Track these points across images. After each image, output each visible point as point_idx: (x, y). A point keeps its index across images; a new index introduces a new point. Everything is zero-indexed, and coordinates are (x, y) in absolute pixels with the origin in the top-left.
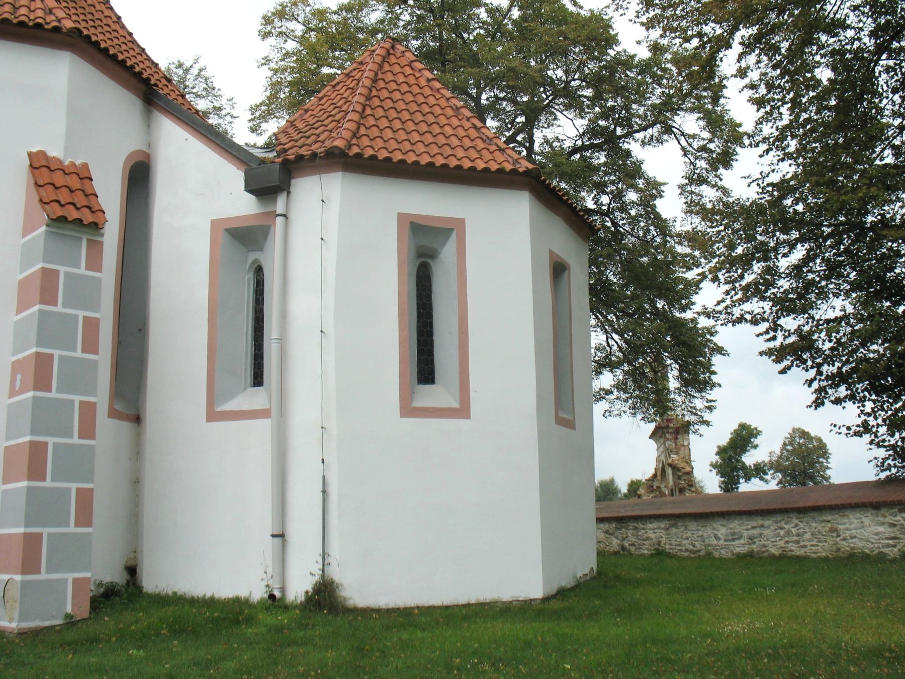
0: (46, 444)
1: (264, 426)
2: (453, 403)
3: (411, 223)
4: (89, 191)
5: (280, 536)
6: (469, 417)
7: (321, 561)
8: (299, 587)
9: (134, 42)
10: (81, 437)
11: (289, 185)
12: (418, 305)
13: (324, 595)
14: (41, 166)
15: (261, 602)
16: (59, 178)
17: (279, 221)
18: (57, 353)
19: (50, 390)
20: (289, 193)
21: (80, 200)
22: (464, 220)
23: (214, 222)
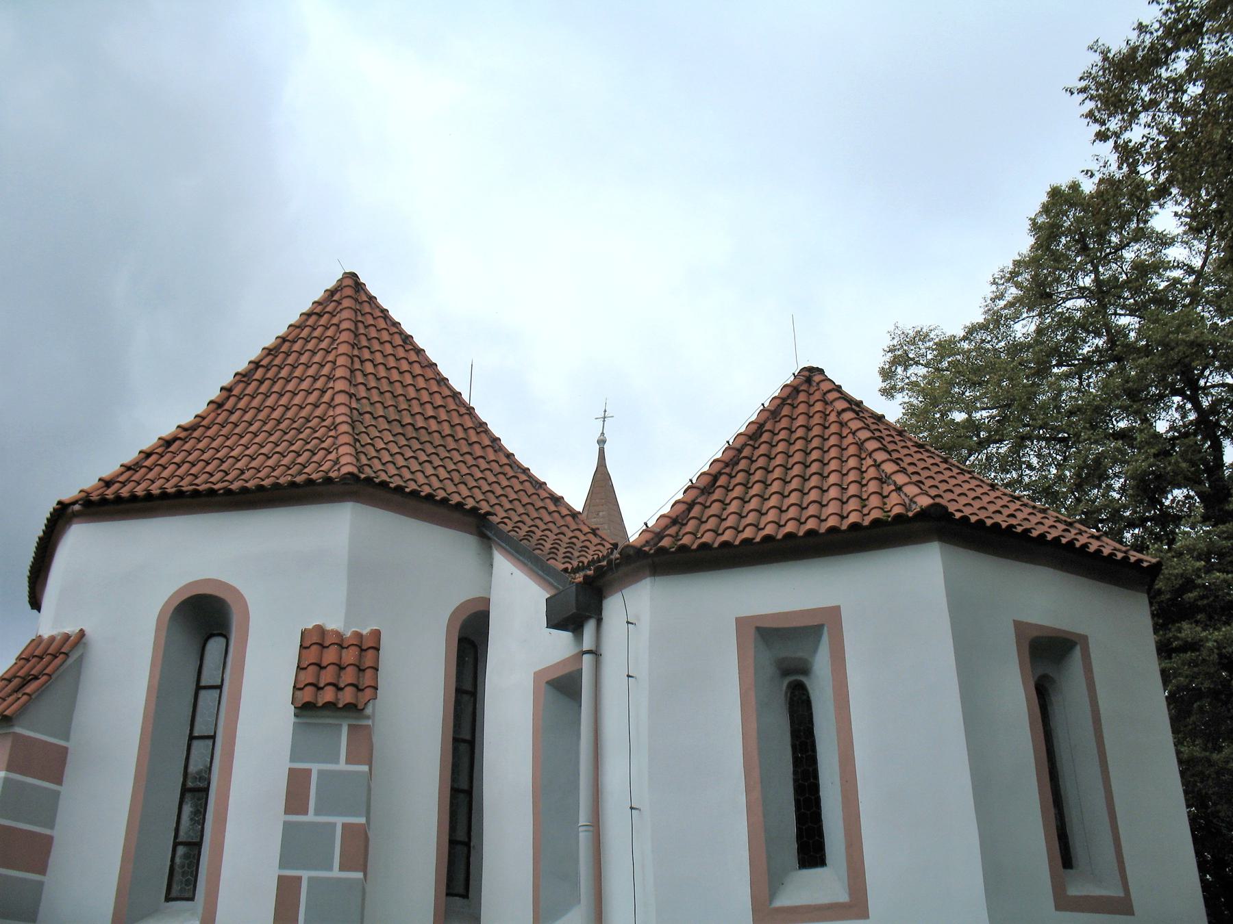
3: (758, 629)
12: (794, 747)
14: (315, 643)
17: (587, 659)
22: (737, 619)
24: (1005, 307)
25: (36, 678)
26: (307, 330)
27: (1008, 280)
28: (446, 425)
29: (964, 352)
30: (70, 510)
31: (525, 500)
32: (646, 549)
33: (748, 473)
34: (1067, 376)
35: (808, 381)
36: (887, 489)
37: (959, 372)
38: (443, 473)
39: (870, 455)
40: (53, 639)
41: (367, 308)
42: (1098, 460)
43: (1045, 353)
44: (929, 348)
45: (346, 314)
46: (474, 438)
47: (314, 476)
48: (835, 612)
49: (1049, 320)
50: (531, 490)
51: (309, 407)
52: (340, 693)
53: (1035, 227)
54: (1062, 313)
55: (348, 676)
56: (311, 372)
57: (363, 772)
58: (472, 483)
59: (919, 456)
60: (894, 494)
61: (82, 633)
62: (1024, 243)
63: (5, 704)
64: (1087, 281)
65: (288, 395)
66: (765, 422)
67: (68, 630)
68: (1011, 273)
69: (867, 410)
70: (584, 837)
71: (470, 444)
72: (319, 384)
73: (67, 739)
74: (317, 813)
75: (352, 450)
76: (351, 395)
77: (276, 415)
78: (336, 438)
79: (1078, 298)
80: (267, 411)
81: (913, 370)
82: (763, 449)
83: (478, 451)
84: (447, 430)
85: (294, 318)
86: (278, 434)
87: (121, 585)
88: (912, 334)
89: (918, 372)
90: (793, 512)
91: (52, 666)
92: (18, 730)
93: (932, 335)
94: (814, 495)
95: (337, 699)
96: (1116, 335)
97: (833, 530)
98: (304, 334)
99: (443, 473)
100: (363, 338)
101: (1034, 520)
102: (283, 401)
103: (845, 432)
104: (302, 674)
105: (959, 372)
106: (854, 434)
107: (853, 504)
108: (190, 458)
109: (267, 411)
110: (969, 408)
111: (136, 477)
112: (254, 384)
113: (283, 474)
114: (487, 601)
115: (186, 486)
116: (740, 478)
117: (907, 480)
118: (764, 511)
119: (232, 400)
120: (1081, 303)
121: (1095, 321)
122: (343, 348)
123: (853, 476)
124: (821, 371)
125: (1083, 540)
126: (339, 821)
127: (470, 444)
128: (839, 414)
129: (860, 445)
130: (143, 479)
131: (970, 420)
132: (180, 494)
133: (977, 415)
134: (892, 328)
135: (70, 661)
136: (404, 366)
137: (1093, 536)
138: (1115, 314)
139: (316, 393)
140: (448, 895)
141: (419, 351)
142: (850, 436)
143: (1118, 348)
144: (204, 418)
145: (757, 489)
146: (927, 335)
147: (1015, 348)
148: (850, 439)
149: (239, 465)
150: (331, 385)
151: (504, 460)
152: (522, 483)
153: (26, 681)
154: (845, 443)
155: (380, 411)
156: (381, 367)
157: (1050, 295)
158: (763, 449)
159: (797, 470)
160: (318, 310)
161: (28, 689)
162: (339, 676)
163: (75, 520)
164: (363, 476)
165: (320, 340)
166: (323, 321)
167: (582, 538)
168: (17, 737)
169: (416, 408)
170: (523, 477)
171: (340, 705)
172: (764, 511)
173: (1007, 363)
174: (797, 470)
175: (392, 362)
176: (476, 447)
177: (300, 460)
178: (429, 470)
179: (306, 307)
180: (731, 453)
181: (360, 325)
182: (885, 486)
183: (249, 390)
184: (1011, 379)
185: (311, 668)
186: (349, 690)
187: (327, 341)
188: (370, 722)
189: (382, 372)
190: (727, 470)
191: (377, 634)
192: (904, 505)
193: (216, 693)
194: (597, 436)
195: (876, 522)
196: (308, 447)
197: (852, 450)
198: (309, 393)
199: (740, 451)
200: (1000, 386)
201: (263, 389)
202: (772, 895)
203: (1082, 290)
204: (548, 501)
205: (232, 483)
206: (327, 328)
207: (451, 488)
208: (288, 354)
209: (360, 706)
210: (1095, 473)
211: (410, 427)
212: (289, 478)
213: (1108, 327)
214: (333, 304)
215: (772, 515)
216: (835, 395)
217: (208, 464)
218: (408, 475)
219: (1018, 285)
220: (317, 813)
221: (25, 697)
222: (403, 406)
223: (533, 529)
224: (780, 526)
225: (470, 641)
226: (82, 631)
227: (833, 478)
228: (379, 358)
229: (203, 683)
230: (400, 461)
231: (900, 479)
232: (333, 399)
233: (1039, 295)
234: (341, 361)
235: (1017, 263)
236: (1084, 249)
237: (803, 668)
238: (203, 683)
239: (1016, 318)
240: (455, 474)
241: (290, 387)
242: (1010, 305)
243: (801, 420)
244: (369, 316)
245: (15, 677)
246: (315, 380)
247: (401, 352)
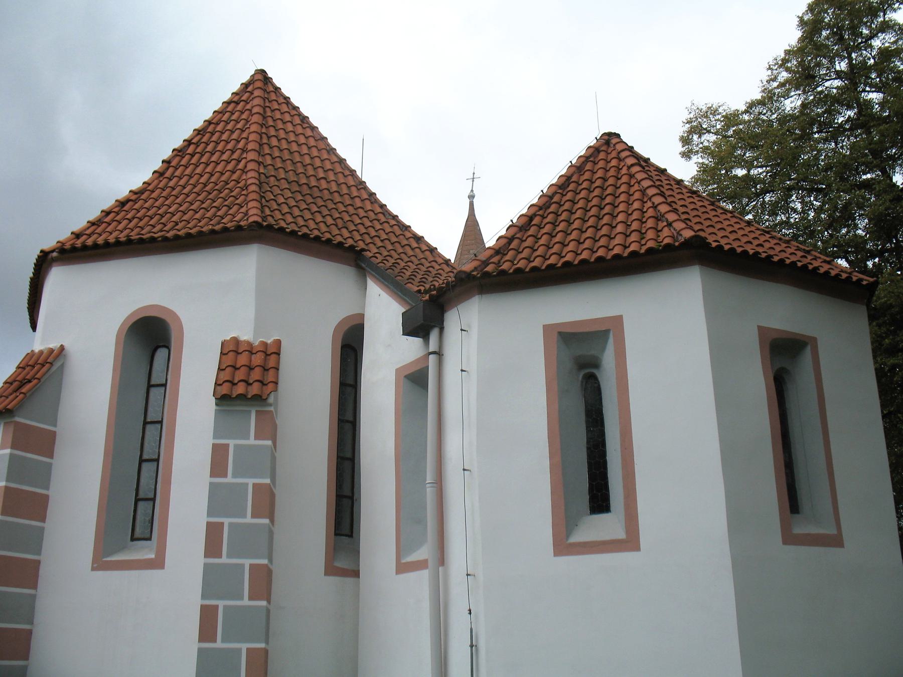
0: (217, 607)
2: (620, 534)
3: (560, 333)
14: (232, 350)
19: (220, 557)
20: (442, 329)
24: (778, 87)
25: (30, 381)
26: (227, 115)
27: (780, 66)
28: (333, 184)
29: (745, 122)
30: (50, 256)
31: (394, 239)
32: (475, 273)
33: (557, 215)
34: (826, 140)
35: (607, 143)
36: (661, 225)
37: (740, 138)
38: (329, 220)
39: (650, 199)
40: (41, 352)
41: (273, 96)
42: (846, 206)
44: (718, 120)
45: (257, 101)
46: (355, 194)
47: (228, 225)
48: (619, 320)
49: (812, 98)
50: (398, 232)
51: (228, 173)
52: (250, 388)
53: (802, 22)
54: (822, 92)
55: (256, 374)
56: (230, 146)
57: (267, 446)
58: (352, 227)
59: (691, 200)
60: (666, 229)
61: (62, 348)
62: (792, 36)
63: (8, 400)
64: (842, 66)
65: (212, 165)
66: (572, 175)
67: (51, 346)
68: (782, 60)
69: (653, 165)
70: (430, 492)
71: (352, 198)
72: (235, 156)
73: (55, 426)
75: (258, 205)
76: (259, 163)
77: (203, 180)
78: (246, 195)
79: (835, 79)
80: (196, 177)
81: (706, 137)
82: (569, 196)
83: (358, 203)
84: (334, 187)
85: (218, 106)
86: (204, 194)
87: (90, 313)
88: (704, 109)
89: (710, 139)
90: (588, 243)
91: (40, 374)
92: (17, 419)
93: (720, 110)
94: (605, 230)
95: (247, 392)
96: (865, 107)
97: (617, 257)
98: (225, 118)
99: (329, 220)
100: (270, 119)
101: (778, 248)
102: (209, 169)
103: (633, 182)
104: (222, 374)
105: (740, 138)
106: (639, 183)
107: (634, 237)
108: (139, 215)
109: (196, 177)
110: (749, 165)
111: (99, 230)
112: (187, 157)
113: (207, 224)
114: (362, 316)
115: (134, 236)
116: (550, 218)
117: (676, 217)
118: (566, 243)
119: (171, 170)
120: (837, 83)
121: (850, 95)
122: (254, 128)
123: (636, 215)
124: (618, 136)
125: (816, 264)
126: (251, 482)
127: (352, 198)
129: (643, 192)
130: (104, 231)
131: (747, 176)
132: (129, 241)
133: (754, 172)
134: (689, 105)
135: (54, 368)
136: (302, 140)
137: (825, 261)
138: (864, 91)
139: (233, 162)
140: (336, 534)
142: (637, 185)
143: (865, 119)
144: (149, 184)
145: (562, 226)
146: (717, 110)
147: (784, 119)
148: (636, 187)
149: (174, 219)
150: (244, 156)
151: (379, 210)
152: (392, 226)
153: (23, 384)
154: (632, 190)
155: (282, 175)
156: (284, 141)
157: (814, 77)
158: (569, 196)
159: (594, 211)
160: (236, 99)
161: (24, 390)
162: (249, 374)
163: (54, 264)
164: (265, 224)
165: (237, 122)
166: (239, 107)
167: (437, 267)
169: (311, 172)
170: (393, 222)
171: (249, 396)
172: (566, 243)
173: (779, 130)
174: (594, 211)
175: (292, 137)
176: (357, 200)
177: (219, 213)
178: (319, 218)
179: (227, 96)
180: (545, 199)
181: (267, 109)
182: (660, 223)
183: (183, 162)
184: (780, 143)
185: (228, 369)
186: (256, 385)
187: (242, 122)
188: (272, 409)
189: (284, 145)
190: (541, 212)
191: (278, 343)
192: (673, 237)
193: (162, 389)
194: (468, 192)
195: (650, 251)
196: (226, 203)
197: (637, 195)
198: (228, 162)
199: (551, 197)
200: (772, 148)
201: (194, 161)
202: (568, 534)
203: (837, 72)
204: (411, 240)
205: (168, 232)
206: (242, 113)
207: (335, 231)
208: (212, 134)
209: (264, 397)
210: (847, 217)
211: (305, 186)
212: (210, 227)
213: (857, 100)
214: (247, 94)
215: (572, 246)
216: (627, 153)
217: (152, 218)
218: (302, 223)
219: (788, 70)
221: (22, 395)
222: (301, 170)
223: (398, 261)
224: (577, 254)
225: (350, 346)
226: (62, 346)
227: (621, 217)
228: (282, 134)
229: (153, 382)
230: (296, 212)
231: (671, 217)
232: (246, 166)
235: (787, 52)
236: (841, 39)
238: (153, 382)
239: (786, 96)
240: (339, 221)
241: (214, 158)
242: (782, 85)
243: (600, 174)
244: (275, 103)
245: (15, 381)
246: (233, 152)
247: (299, 130)
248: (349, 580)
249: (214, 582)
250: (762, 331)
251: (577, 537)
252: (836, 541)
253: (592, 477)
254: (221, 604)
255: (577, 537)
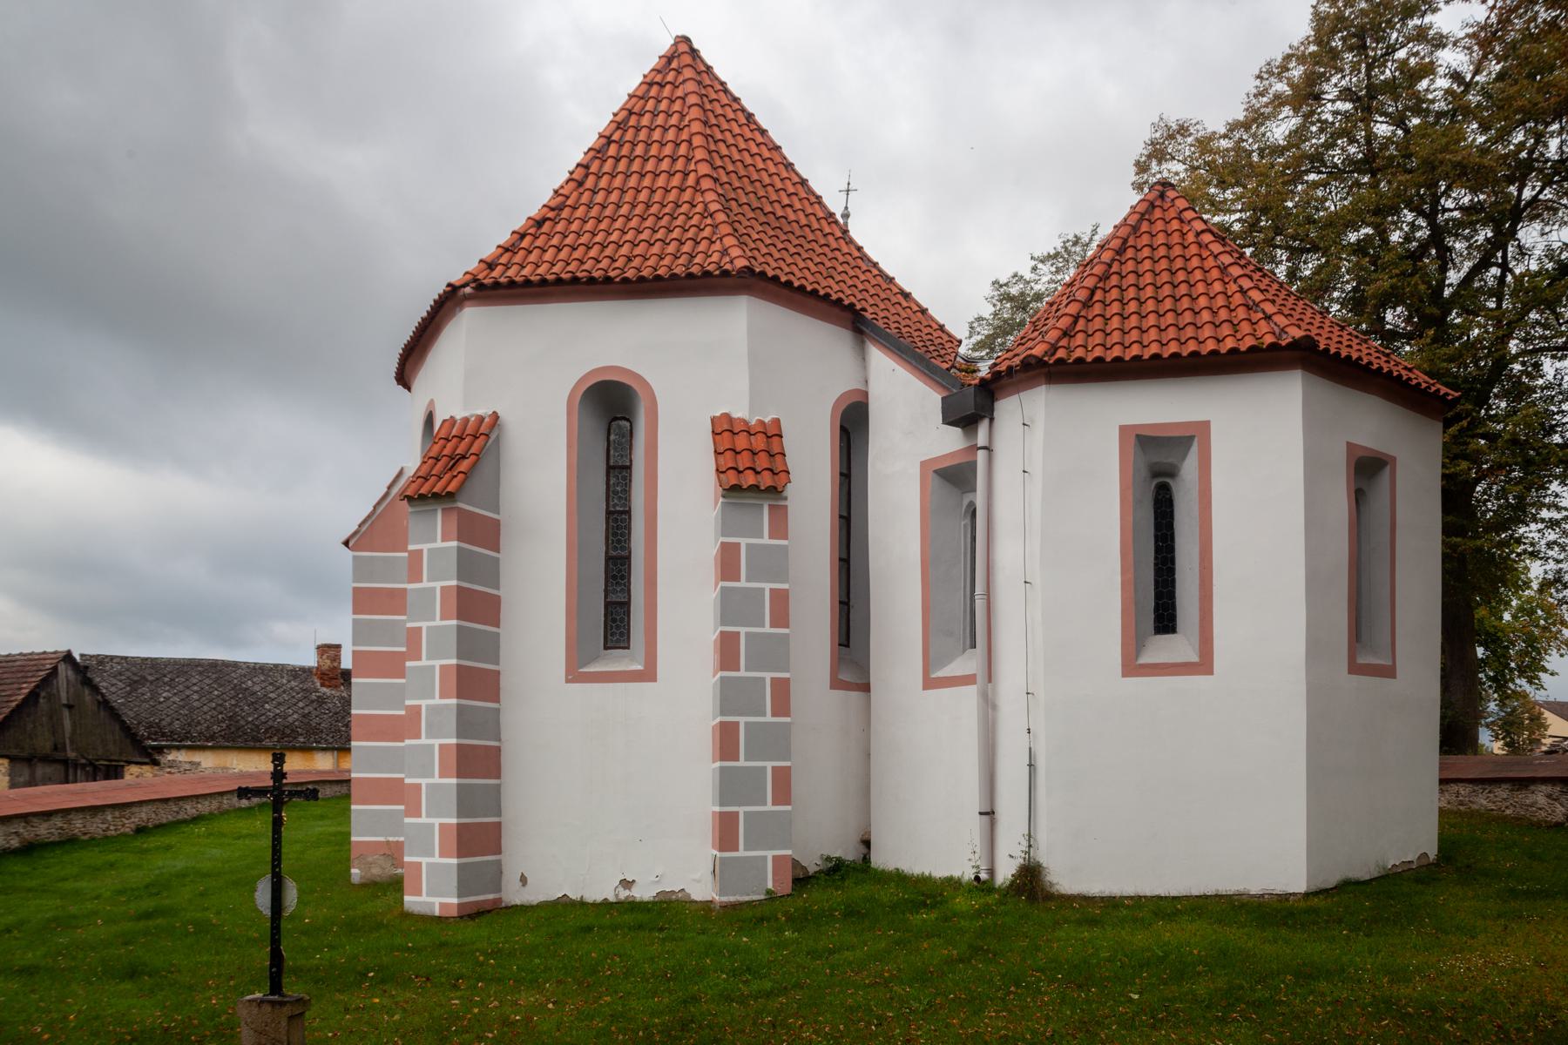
0: (737, 723)
1: (970, 693)
4: (776, 450)
5: (989, 814)
6: (1125, 675)
7: (1025, 843)
8: (1005, 872)
9: (864, 257)
10: (774, 714)
11: (992, 410)
12: (1156, 537)
13: (1030, 875)
14: (725, 430)
15: (969, 883)
16: (741, 442)
17: (981, 455)
18: (743, 630)
20: (992, 420)
21: (762, 462)
23: (923, 464)
25: (464, 457)
29: (1218, 151)
40: (466, 420)
43: (1303, 157)
48: (1205, 426)
67: (480, 412)
74: (748, 580)
92: (460, 505)
114: (866, 394)
128: (1198, 234)
129: (1223, 269)
134: (1156, 120)
141: (763, 132)
150: (692, 167)
160: (658, 79)
168: (460, 511)
191: (777, 422)
197: (1215, 274)
202: (1138, 653)
214: (672, 74)
220: (748, 580)
233: (1307, 96)
234: (697, 141)
237: (1172, 472)
248: (855, 696)
249: (731, 697)
250: (1351, 447)
251: (1145, 659)
252: (1389, 672)
253: (1161, 595)
254: (742, 720)
255: (1145, 659)
